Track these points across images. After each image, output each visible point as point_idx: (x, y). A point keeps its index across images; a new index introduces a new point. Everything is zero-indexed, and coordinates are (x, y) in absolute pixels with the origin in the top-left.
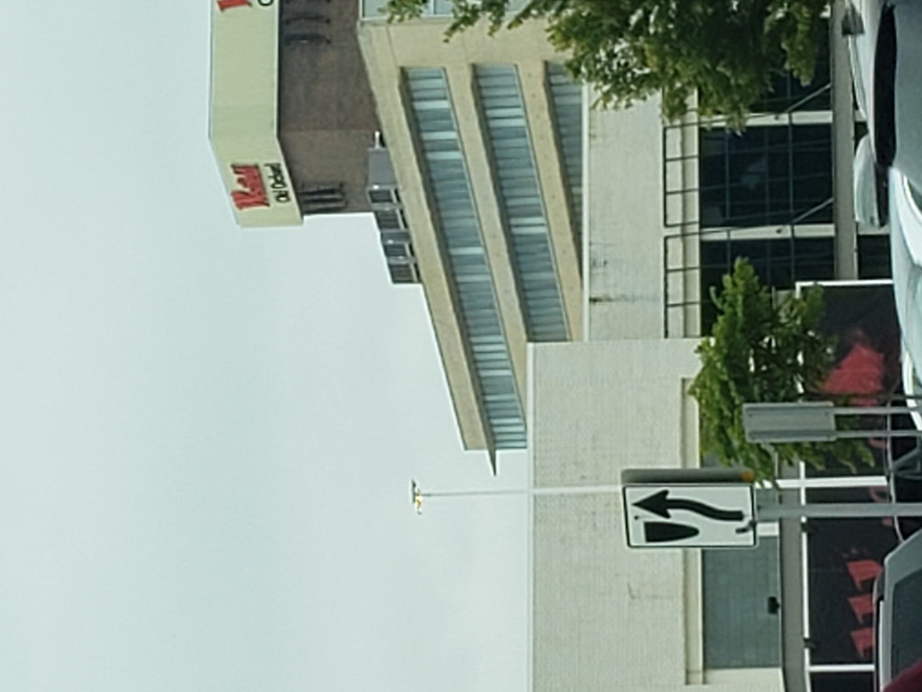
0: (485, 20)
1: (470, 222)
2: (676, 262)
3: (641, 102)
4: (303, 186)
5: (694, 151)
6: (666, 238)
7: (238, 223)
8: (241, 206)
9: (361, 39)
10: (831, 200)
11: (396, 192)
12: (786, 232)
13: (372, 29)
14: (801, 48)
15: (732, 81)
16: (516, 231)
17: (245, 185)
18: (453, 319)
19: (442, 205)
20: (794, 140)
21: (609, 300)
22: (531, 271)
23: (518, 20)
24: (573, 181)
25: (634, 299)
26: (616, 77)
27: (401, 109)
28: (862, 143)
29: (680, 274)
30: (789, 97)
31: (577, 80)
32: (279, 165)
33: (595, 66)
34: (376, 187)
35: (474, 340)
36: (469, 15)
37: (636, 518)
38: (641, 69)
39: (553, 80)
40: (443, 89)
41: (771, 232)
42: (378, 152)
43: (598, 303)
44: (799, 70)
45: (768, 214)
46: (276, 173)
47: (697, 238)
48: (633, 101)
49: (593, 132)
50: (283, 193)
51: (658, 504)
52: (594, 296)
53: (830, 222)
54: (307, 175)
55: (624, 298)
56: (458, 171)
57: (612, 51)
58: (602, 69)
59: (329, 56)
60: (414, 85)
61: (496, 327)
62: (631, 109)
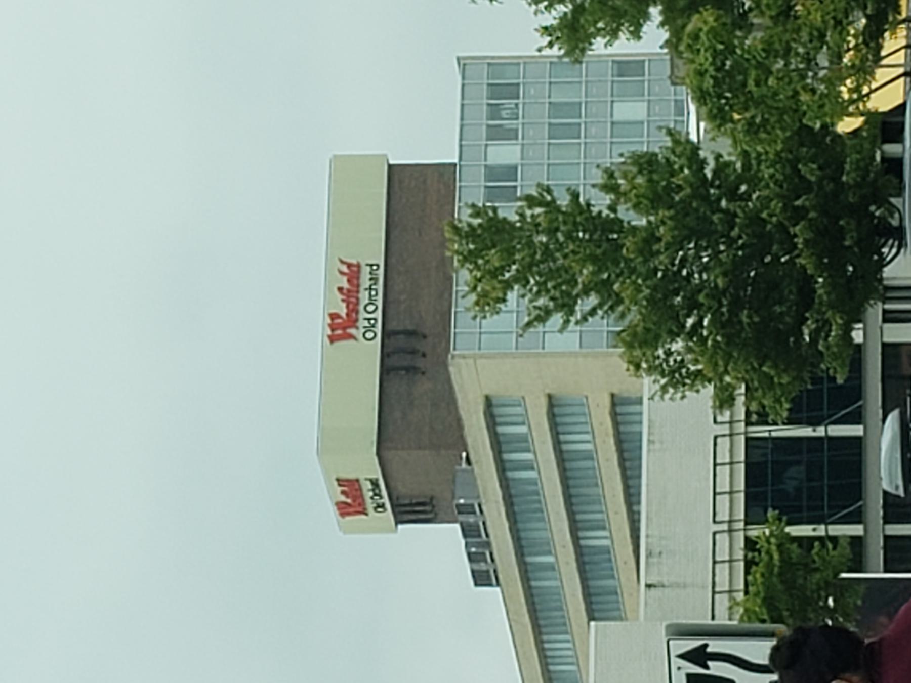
0: (557, 319)
1: (543, 534)
2: (723, 554)
3: (695, 394)
4: (398, 499)
5: (741, 457)
6: (714, 534)
7: (340, 529)
8: (343, 515)
9: (452, 369)
10: (860, 503)
11: (480, 506)
12: (821, 530)
13: (462, 361)
14: (835, 349)
15: (776, 380)
16: (582, 542)
17: (347, 496)
18: (527, 619)
19: (519, 518)
20: (829, 450)
21: (663, 586)
22: (594, 579)
23: (585, 319)
24: (634, 499)
25: (685, 586)
26: (672, 372)
27: (485, 432)
28: (890, 418)
29: (727, 438)
30: (825, 412)
31: (638, 374)
32: (377, 480)
33: (654, 362)
34: (462, 501)
35: (545, 638)
36: (542, 314)
37: (679, 668)
38: (694, 365)
39: (619, 409)
40: (521, 415)
41: (807, 530)
42: (464, 471)
43: (652, 589)
44: (835, 369)
45: (805, 514)
46: (375, 486)
47: (742, 534)
48: (687, 393)
49: (652, 438)
50: (381, 505)
51: (699, 656)
52: (649, 582)
53: (859, 522)
54: (401, 489)
55: (677, 585)
56: (533, 488)
57: (669, 349)
58: (661, 365)
59: (423, 386)
60: (497, 411)
61: (563, 627)
62: (685, 400)
